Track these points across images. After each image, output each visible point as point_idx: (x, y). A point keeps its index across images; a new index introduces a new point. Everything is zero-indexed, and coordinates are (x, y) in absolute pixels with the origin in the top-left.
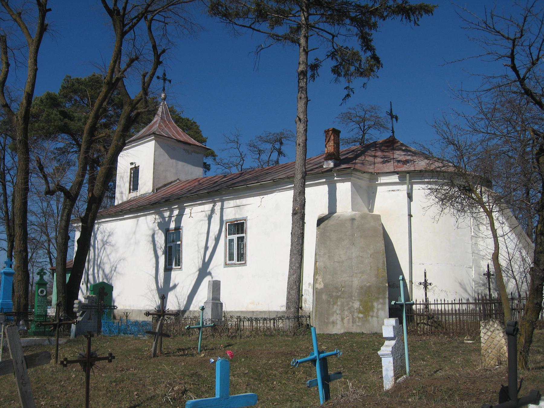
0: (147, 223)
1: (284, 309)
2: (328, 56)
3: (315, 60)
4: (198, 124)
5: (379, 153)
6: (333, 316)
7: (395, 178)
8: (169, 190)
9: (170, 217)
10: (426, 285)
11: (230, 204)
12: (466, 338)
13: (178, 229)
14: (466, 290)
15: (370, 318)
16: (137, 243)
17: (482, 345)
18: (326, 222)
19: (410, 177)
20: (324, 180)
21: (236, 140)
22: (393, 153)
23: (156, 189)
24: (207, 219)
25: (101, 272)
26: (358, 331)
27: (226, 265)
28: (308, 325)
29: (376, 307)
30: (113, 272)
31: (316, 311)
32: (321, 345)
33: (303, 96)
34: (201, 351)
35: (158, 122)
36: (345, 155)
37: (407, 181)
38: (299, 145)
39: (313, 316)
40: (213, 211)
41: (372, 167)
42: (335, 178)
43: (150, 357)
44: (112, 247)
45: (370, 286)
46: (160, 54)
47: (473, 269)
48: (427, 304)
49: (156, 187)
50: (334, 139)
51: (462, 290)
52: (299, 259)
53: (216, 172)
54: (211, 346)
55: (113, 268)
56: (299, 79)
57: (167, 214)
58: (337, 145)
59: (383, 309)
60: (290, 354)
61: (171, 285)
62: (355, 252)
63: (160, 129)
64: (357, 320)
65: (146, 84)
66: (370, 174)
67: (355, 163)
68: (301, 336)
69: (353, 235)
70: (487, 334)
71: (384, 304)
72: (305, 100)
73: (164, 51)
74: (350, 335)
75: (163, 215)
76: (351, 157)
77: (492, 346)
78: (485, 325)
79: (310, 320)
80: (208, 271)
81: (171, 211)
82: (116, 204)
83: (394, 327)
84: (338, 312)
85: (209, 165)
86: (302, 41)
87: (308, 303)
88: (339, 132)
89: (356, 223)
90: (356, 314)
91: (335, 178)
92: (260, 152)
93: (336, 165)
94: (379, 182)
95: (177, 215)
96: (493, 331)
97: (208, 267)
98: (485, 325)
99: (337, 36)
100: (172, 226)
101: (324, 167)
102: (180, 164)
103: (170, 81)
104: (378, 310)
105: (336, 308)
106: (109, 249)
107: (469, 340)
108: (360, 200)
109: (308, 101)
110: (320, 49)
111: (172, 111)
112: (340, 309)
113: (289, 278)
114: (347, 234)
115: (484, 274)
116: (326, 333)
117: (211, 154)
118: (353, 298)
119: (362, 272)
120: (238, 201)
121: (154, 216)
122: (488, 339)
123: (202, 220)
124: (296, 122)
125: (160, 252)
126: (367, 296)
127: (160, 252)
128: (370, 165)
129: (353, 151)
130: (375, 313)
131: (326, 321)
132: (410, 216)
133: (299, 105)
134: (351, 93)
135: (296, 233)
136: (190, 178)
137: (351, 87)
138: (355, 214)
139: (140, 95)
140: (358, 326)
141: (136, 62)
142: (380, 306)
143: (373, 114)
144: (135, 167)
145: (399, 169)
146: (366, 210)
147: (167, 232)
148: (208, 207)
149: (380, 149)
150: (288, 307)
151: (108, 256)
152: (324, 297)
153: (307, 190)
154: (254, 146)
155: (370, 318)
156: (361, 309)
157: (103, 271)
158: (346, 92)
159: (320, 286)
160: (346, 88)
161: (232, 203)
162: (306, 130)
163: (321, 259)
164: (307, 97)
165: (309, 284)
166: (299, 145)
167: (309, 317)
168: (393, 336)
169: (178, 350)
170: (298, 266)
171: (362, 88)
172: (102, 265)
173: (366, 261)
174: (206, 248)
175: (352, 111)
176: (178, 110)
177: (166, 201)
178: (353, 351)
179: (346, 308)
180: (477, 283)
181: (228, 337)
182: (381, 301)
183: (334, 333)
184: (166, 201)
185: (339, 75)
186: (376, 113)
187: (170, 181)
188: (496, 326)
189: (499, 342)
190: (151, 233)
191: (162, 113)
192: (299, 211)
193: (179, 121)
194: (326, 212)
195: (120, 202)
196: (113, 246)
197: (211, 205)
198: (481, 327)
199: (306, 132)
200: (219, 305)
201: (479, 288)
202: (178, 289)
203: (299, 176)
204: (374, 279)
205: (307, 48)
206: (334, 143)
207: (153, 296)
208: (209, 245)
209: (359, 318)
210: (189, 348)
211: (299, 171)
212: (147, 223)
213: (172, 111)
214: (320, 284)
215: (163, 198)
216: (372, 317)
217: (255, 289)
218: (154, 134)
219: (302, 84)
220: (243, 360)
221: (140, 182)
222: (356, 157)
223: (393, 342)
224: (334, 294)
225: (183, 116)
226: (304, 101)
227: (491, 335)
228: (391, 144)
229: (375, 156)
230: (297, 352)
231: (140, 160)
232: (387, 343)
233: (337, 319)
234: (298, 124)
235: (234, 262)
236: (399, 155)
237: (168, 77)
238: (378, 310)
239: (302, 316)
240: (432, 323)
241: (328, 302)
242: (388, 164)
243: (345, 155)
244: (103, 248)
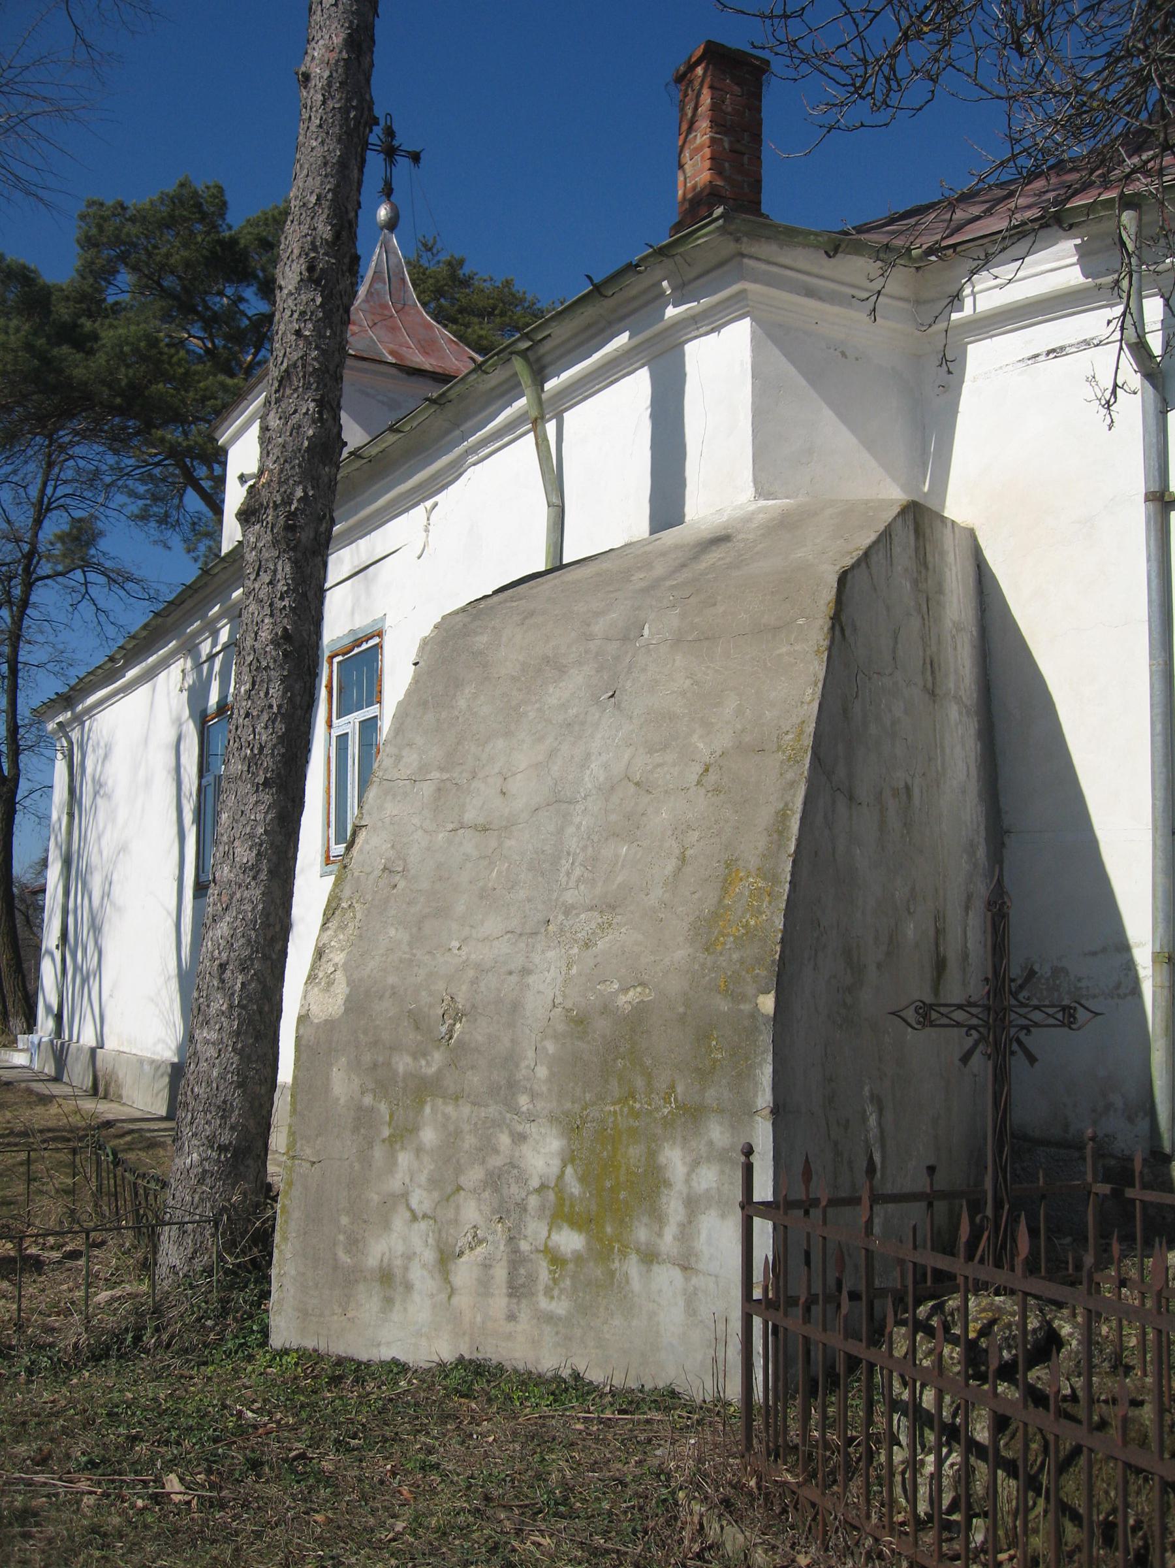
6: (386, 1225)
15: (632, 1267)
26: (548, 1360)
29: (679, 1185)
45: (641, 1011)
50: (714, 107)
62: (608, 749)
84: (420, 1199)
90: (536, 1230)
103: (416, 157)
104: (693, 1204)
105: (409, 1172)
112: (434, 1183)
116: (340, 1348)
118: (523, 1101)
131: (344, 1258)
132: (1117, 368)
155: (632, 1267)
156: (574, 1188)
179: (473, 1176)
182: (717, 1133)
183: (386, 1354)
197: (636, 388)
204: (681, 954)
209: (556, 1259)
216: (650, 1257)
224: (403, 1063)
233: (409, 1257)
237: (403, 141)
238: (693, 1204)
241: (363, 1119)
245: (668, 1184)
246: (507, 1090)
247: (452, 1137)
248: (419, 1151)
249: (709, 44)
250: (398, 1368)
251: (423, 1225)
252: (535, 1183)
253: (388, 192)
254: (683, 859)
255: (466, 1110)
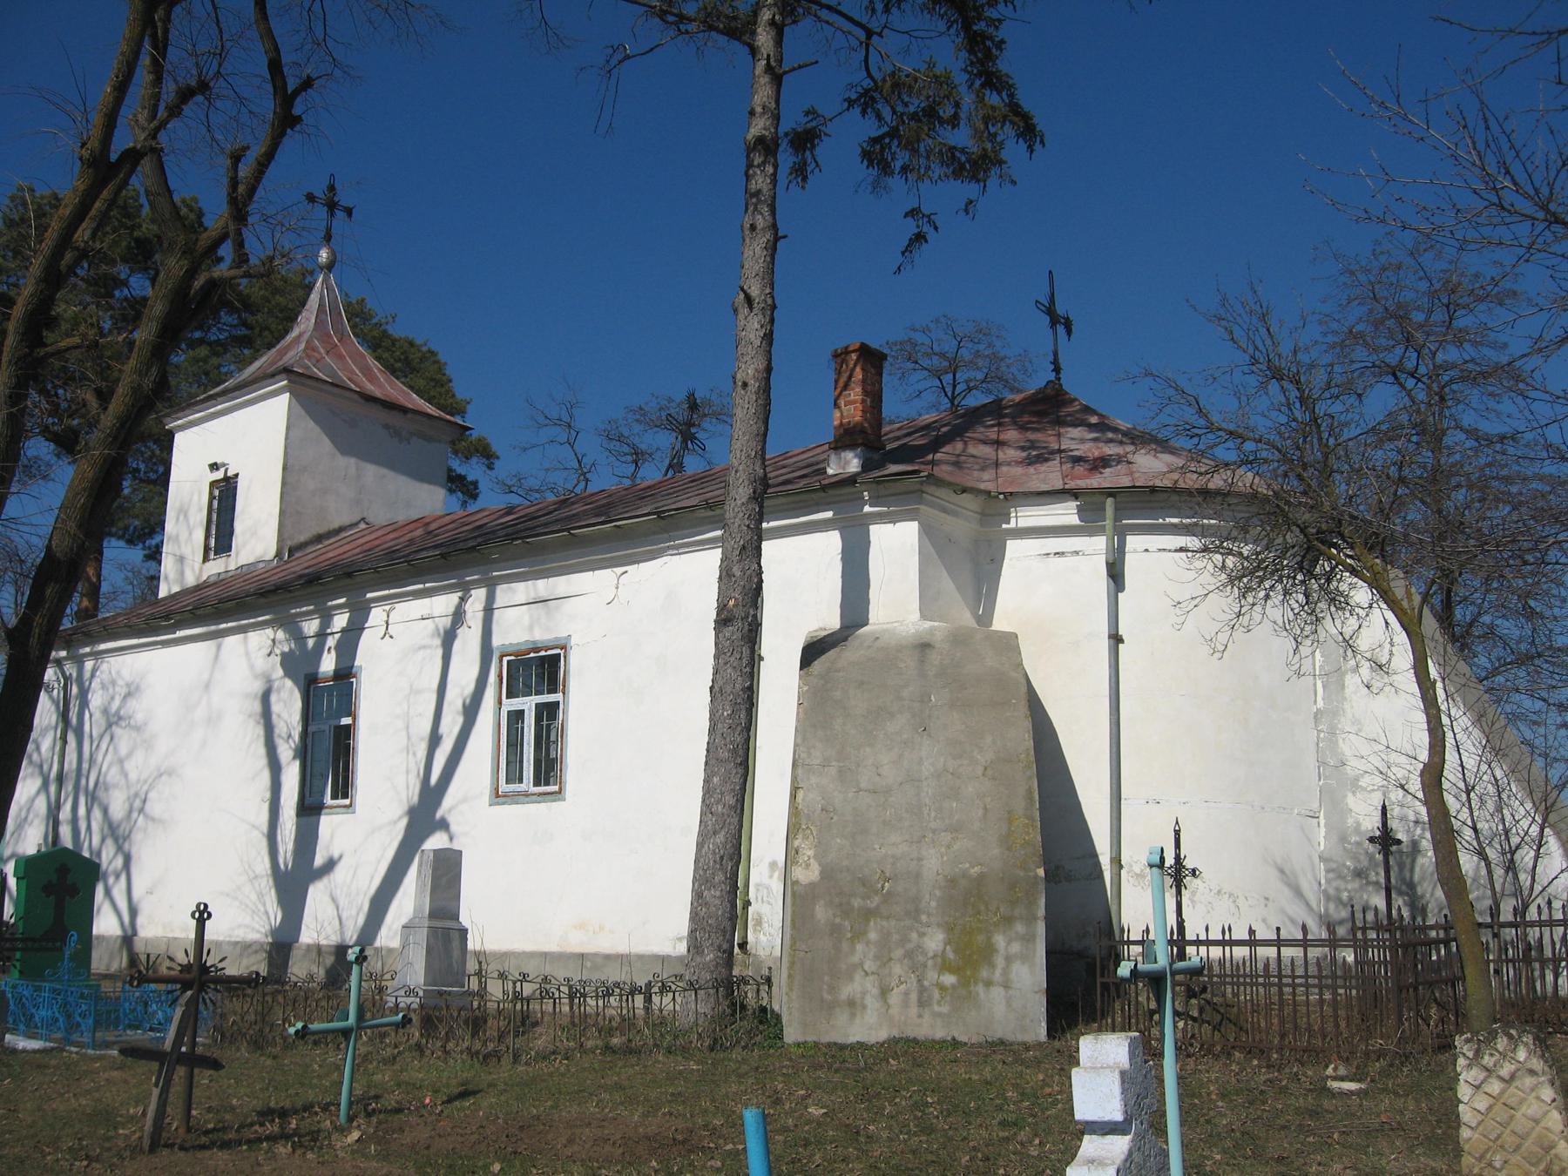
0: (247, 654)
1: (682, 948)
2: (851, 103)
3: (807, 113)
4: (442, 358)
5: (1011, 434)
6: (851, 979)
7: (1066, 513)
8: (331, 552)
9: (322, 635)
10: (1177, 874)
11: (514, 593)
12: (1330, 1071)
13: (345, 674)
14: (1298, 892)
16: (213, 720)
17: (1465, 1133)
18: (832, 653)
19: (1116, 509)
20: (829, 514)
21: (566, 418)
22: (1059, 435)
23: (289, 549)
24: (438, 642)
25: (97, 814)
26: (940, 1034)
27: (498, 796)
28: (763, 1010)
30: (135, 815)
31: (792, 964)
32: (804, 1098)
33: (760, 222)
34: (351, 1119)
35: (306, 336)
36: (898, 438)
37: (1109, 523)
38: (745, 385)
39: (781, 980)
40: (458, 616)
41: (986, 476)
42: (867, 509)
43: (136, 1150)
44: (134, 734)
45: (981, 877)
46: (296, 93)
47: (1322, 822)
48: (1179, 942)
49: (289, 543)
50: (864, 381)
51: (1286, 890)
52: (737, 780)
53: (491, 501)
54: (391, 1101)
55: (137, 803)
56: (750, 166)
57: (311, 627)
58: (874, 398)
59: (1026, 958)
60: (683, 1142)
61: (319, 861)
62: (929, 757)
63: (309, 357)
64: (936, 994)
65: (241, 189)
66: (982, 497)
67: (933, 463)
68: (737, 1054)
69: (924, 699)
70: (1487, 1088)
71: (1029, 939)
72: (769, 235)
73: (307, 84)
74: (905, 1048)
75: (300, 630)
76: (925, 441)
77: (1508, 1139)
78: (1478, 1054)
79: (769, 993)
80: (438, 815)
81: (326, 619)
82: (163, 593)
83: (1123, 1073)
85: (475, 484)
86: (764, 39)
87: (767, 929)
88: (883, 357)
89: (934, 658)
90: (932, 975)
91: (867, 509)
92: (638, 457)
93: (867, 467)
94: (1012, 525)
95: (343, 631)
96: (1513, 1077)
97: (438, 803)
98: (1478, 1054)
99: (880, 35)
100: (328, 664)
101: (830, 471)
102: (371, 471)
103: (349, 212)
106: (124, 738)
107: (1342, 1079)
108: (947, 584)
109: (777, 239)
110: (827, 72)
111: (358, 315)
112: (877, 957)
113: (700, 845)
114: (905, 693)
115: (1372, 840)
116: (826, 1039)
117: (486, 453)
118: (924, 918)
119: (955, 829)
120: (541, 583)
121: (269, 632)
122: (1490, 1108)
123: (424, 647)
124: (736, 311)
125: (286, 752)
126: (971, 910)
127: (286, 752)
128: (983, 469)
129: (927, 427)
130: (998, 972)
131: (827, 997)
132: (1116, 639)
133: (748, 253)
134: (927, 229)
135: (729, 689)
136: (402, 516)
137: (926, 210)
138: (932, 629)
139: (221, 223)
140: (940, 1015)
141: (200, 98)
142: (1016, 947)
143: (981, 347)
144: (226, 479)
145: (1082, 483)
146: (966, 619)
147: (309, 684)
148: (444, 604)
149: (1015, 423)
150: (695, 946)
151: (121, 761)
152: (821, 913)
153: (767, 547)
154: (620, 439)
155: (980, 989)
156: (951, 955)
157: (105, 811)
158: (911, 227)
159: (807, 874)
160: (913, 213)
161: (521, 591)
162: (768, 338)
163: (814, 780)
164: (774, 226)
165: (773, 865)
166: (745, 385)
167: (769, 981)
168: (1119, 1117)
169: (261, 1114)
170: (732, 802)
171: (962, 213)
172: (101, 793)
173: (970, 789)
174: (435, 740)
175: (920, 338)
176: (379, 307)
177: (317, 583)
178: (929, 1130)
179: (898, 953)
180: (1335, 872)
181: (473, 1054)
182: (1020, 928)
183: (852, 1039)
184: (317, 583)
185: (886, 169)
186: (990, 345)
187: (336, 525)
188: (1522, 1055)
189: (1537, 1122)
190: (258, 687)
191: (321, 305)
192: (739, 612)
193: (379, 343)
194: (833, 622)
195: (176, 589)
196: (138, 729)
197: (453, 599)
198: (1461, 1061)
199: (771, 344)
200: (455, 935)
201: (1342, 885)
202: (339, 873)
203: (741, 492)
204: (996, 851)
205: (780, 61)
206: (865, 392)
207: (260, 895)
208: (443, 729)
209: (942, 988)
210: (307, 1108)
211: (742, 476)
212: (249, 655)
213: (358, 315)
214: (808, 866)
215: (301, 576)
216: (988, 984)
217: (583, 880)
218: (287, 371)
219: (760, 182)
220: (497, 1167)
221: (239, 526)
222: (936, 445)
223: (1120, 1145)
225: (396, 331)
226: (763, 239)
227: (1503, 1092)
228: (1050, 406)
229: (999, 444)
230: (714, 1131)
231: (239, 452)
232: (1090, 1145)
233: (864, 993)
234: (741, 317)
235: (522, 787)
236: (1076, 440)
237: (344, 199)
238: (1009, 959)
239: (744, 980)
240: (1201, 1010)
241: (835, 930)
242: (1043, 468)
243: (898, 438)
244: (106, 739)
245: (997, 951)
246: (914, 914)
247: (885, 936)
248: (868, 943)
249: (863, 345)
250: (861, 1046)
251: (871, 978)
252: (931, 954)
253: (328, 238)
254: (985, 809)
255: (893, 923)
